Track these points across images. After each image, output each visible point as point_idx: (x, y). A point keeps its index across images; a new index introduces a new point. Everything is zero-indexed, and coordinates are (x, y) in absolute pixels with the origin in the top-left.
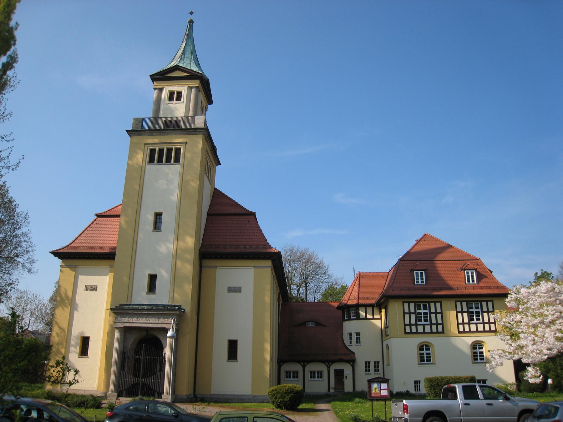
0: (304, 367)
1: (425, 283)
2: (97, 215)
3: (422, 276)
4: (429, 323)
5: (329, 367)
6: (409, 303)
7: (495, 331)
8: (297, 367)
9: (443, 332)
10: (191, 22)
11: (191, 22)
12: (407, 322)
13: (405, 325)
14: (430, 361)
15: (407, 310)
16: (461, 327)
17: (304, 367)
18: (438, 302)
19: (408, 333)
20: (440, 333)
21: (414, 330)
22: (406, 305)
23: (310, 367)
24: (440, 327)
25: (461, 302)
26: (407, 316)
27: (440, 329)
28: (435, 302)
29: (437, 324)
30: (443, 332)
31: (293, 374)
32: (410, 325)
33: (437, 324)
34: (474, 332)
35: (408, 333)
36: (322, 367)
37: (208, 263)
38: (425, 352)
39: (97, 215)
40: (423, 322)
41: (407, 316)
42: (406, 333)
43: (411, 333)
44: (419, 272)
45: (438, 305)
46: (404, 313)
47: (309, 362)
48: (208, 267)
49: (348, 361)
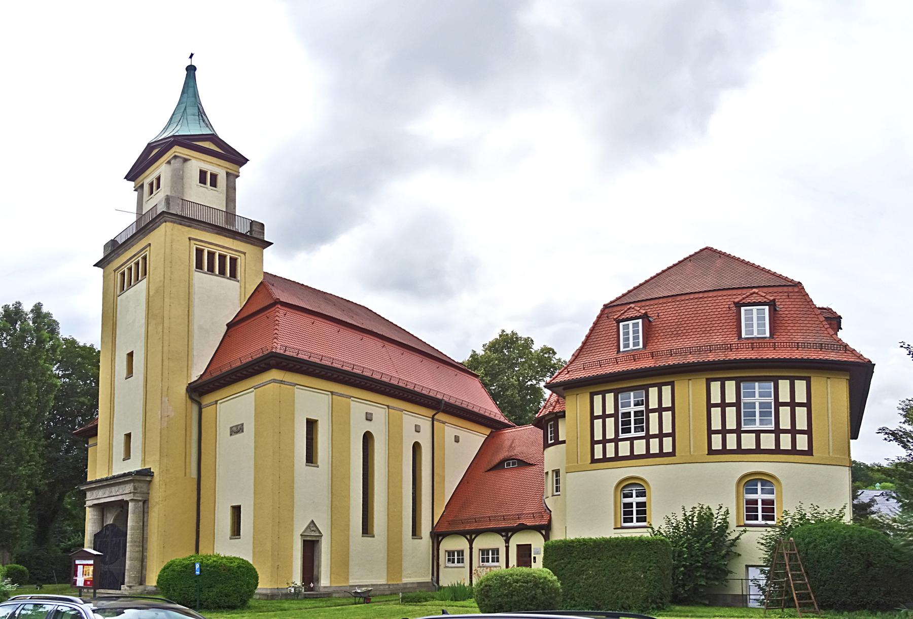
0: (471, 542)
1: (641, 346)
2: (129, 177)
3: (636, 332)
4: (643, 434)
5: (507, 541)
6: (603, 394)
7: (673, 454)
8: (460, 544)
9: (673, 454)
10: (191, 69)
11: (191, 69)
12: (716, 425)
13: (710, 432)
14: (644, 520)
15: (716, 399)
16: (598, 448)
17: (471, 542)
18: (666, 384)
19: (717, 452)
20: (668, 455)
21: (732, 444)
22: (716, 387)
23: (482, 542)
24: (667, 442)
25: (723, 381)
26: (716, 412)
27: (668, 447)
28: (659, 386)
29: (794, 432)
30: (809, 452)
31: (454, 559)
32: (724, 432)
33: (794, 432)
34: (786, 452)
35: (717, 452)
36: (496, 542)
37: (207, 400)
38: (634, 500)
39: (129, 177)
40: (757, 426)
41: (716, 412)
42: (594, 461)
43: (724, 451)
44: (631, 323)
45: (666, 390)
46: (710, 406)
47: (479, 532)
48: (208, 406)
49: (537, 529)
